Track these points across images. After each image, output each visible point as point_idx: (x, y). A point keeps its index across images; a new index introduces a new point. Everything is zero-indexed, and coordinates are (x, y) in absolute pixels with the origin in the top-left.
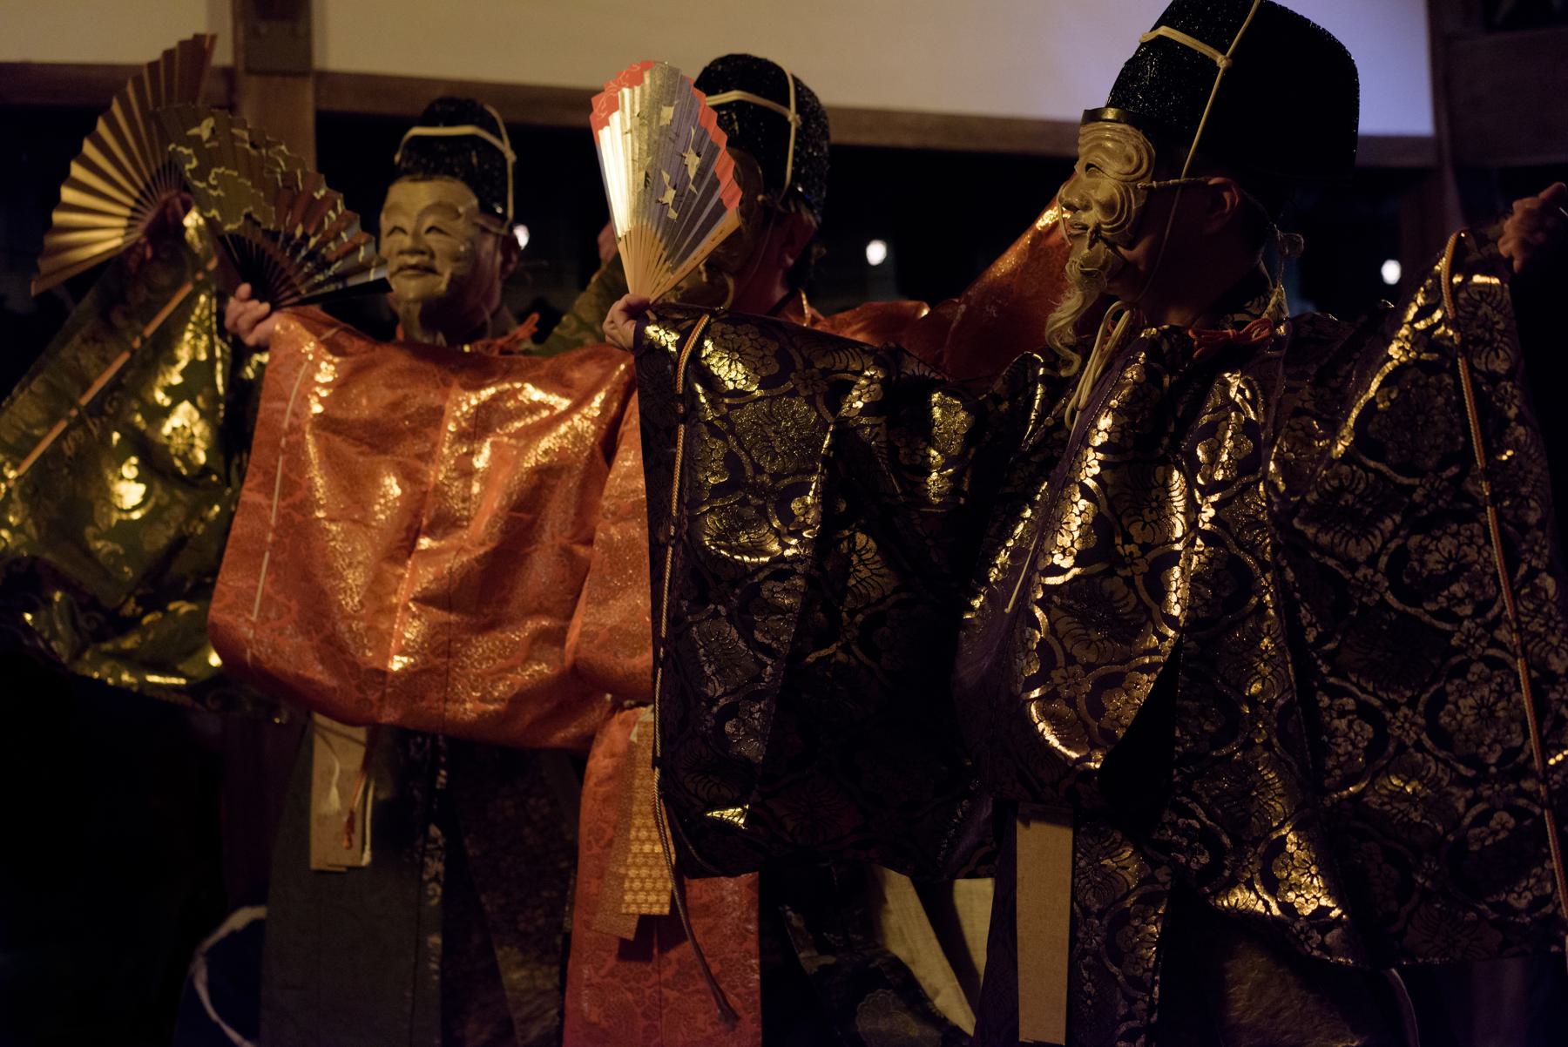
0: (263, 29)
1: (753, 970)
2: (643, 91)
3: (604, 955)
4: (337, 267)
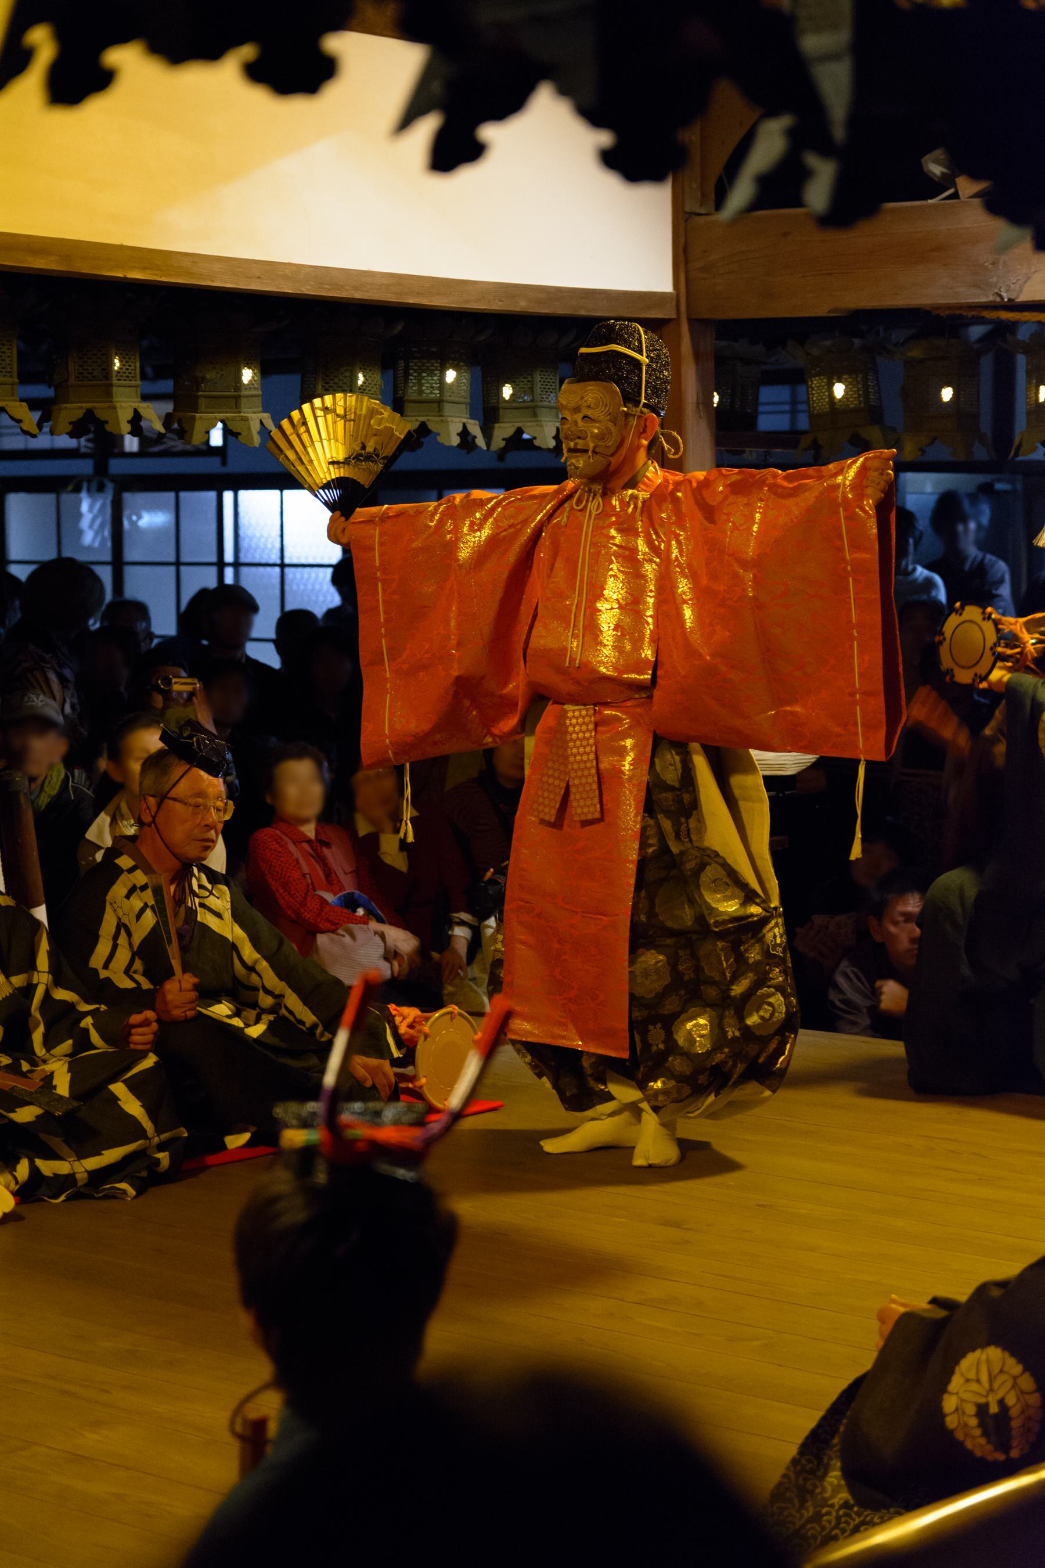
2: (999, 480)
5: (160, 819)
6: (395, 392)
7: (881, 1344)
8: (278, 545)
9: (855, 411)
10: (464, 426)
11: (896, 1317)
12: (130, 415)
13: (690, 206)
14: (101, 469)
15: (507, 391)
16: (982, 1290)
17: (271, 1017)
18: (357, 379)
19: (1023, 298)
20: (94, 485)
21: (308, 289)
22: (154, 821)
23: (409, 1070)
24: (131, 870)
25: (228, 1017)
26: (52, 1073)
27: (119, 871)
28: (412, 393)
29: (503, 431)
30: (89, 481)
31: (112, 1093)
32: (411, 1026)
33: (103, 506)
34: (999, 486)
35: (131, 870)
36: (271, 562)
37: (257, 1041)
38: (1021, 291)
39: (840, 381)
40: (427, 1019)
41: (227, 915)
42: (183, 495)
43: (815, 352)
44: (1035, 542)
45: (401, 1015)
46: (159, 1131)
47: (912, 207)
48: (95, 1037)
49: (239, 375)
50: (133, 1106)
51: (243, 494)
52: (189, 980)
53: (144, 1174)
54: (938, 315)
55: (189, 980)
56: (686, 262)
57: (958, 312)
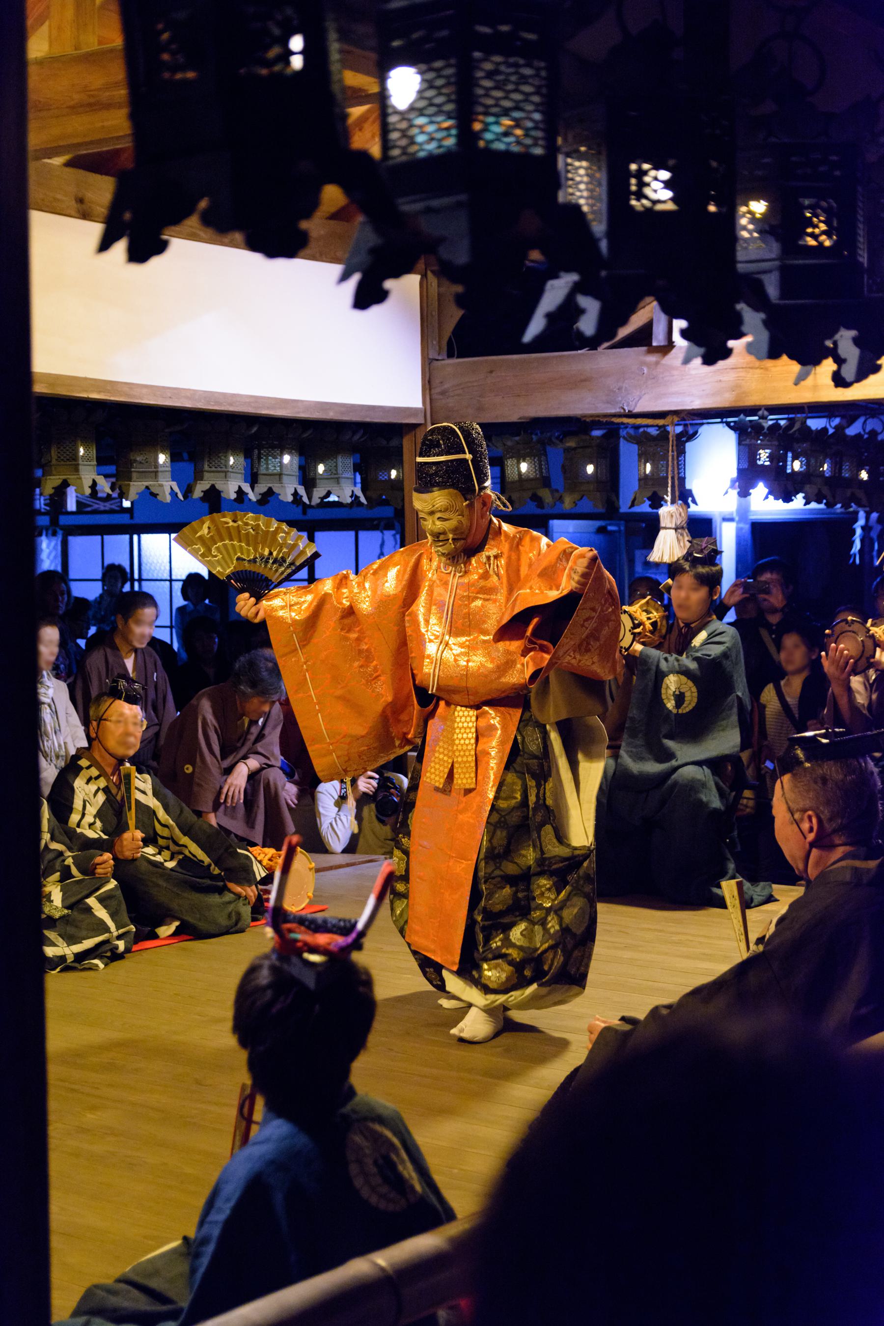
2: (610, 525)
4: (289, 561)
5: (100, 734)
6: (252, 469)
7: (590, 1046)
8: (168, 568)
9: (532, 480)
10: (295, 489)
11: (600, 1030)
12: (90, 483)
13: (433, 354)
14: (54, 522)
15: (321, 468)
16: (655, 1011)
18: (229, 460)
19: (637, 410)
20: (50, 532)
21: (188, 404)
22: (97, 736)
24: (88, 768)
25: (154, 855)
26: (50, 893)
27: (81, 768)
28: (262, 470)
29: (318, 493)
30: (47, 530)
31: (88, 904)
32: (270, 860)
33: (56, 545)
34: (610, 528)
35: (88, 768)
36: (164, 578)
37: (172, 870)
38: (636, 406)
39: (524, 461)
41: (150, 792)
42: (105, 537)
43: (509, 443)
44: (648, 558)
45: (264, 853)
46: (118, 929)
47: (569, 355)
48: (74, 871)
49: (157, 459)
50: (101, 913)
51: (144, 537)
52: (139, 835)
53: (109, 954)
54: (585, 421)
55: (139, 835)
56: (430, 390)
57: (597, 419)
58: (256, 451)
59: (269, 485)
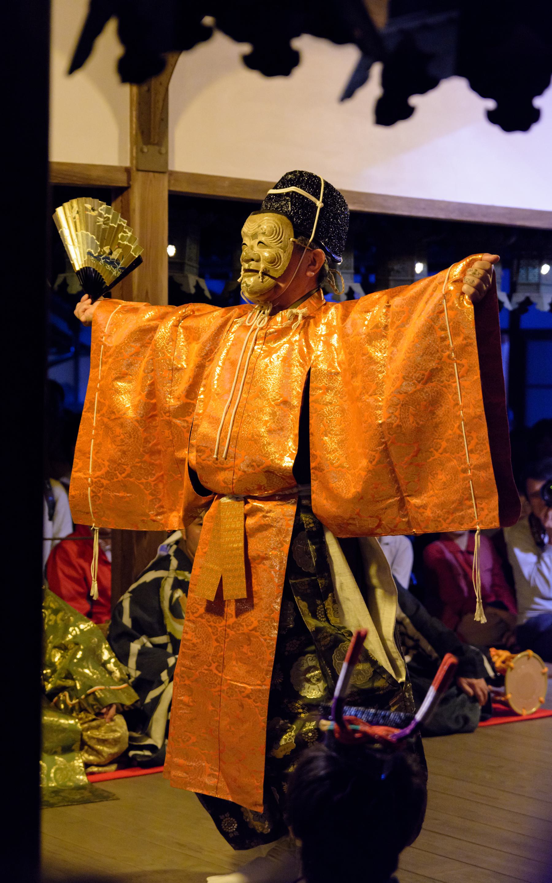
0: (145, 150)
1: (275, 629)
3: (199, 607)
17: (415, 652)
21: (441, 215)
23: (501, 689)
32: (504, 662)
40: (513, 658)
49: (413, 267)
58: (515, 262)
59: (528, 294)
